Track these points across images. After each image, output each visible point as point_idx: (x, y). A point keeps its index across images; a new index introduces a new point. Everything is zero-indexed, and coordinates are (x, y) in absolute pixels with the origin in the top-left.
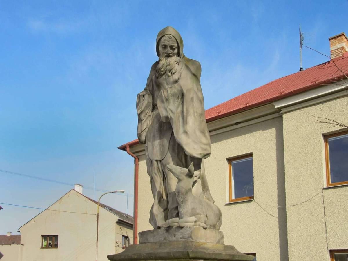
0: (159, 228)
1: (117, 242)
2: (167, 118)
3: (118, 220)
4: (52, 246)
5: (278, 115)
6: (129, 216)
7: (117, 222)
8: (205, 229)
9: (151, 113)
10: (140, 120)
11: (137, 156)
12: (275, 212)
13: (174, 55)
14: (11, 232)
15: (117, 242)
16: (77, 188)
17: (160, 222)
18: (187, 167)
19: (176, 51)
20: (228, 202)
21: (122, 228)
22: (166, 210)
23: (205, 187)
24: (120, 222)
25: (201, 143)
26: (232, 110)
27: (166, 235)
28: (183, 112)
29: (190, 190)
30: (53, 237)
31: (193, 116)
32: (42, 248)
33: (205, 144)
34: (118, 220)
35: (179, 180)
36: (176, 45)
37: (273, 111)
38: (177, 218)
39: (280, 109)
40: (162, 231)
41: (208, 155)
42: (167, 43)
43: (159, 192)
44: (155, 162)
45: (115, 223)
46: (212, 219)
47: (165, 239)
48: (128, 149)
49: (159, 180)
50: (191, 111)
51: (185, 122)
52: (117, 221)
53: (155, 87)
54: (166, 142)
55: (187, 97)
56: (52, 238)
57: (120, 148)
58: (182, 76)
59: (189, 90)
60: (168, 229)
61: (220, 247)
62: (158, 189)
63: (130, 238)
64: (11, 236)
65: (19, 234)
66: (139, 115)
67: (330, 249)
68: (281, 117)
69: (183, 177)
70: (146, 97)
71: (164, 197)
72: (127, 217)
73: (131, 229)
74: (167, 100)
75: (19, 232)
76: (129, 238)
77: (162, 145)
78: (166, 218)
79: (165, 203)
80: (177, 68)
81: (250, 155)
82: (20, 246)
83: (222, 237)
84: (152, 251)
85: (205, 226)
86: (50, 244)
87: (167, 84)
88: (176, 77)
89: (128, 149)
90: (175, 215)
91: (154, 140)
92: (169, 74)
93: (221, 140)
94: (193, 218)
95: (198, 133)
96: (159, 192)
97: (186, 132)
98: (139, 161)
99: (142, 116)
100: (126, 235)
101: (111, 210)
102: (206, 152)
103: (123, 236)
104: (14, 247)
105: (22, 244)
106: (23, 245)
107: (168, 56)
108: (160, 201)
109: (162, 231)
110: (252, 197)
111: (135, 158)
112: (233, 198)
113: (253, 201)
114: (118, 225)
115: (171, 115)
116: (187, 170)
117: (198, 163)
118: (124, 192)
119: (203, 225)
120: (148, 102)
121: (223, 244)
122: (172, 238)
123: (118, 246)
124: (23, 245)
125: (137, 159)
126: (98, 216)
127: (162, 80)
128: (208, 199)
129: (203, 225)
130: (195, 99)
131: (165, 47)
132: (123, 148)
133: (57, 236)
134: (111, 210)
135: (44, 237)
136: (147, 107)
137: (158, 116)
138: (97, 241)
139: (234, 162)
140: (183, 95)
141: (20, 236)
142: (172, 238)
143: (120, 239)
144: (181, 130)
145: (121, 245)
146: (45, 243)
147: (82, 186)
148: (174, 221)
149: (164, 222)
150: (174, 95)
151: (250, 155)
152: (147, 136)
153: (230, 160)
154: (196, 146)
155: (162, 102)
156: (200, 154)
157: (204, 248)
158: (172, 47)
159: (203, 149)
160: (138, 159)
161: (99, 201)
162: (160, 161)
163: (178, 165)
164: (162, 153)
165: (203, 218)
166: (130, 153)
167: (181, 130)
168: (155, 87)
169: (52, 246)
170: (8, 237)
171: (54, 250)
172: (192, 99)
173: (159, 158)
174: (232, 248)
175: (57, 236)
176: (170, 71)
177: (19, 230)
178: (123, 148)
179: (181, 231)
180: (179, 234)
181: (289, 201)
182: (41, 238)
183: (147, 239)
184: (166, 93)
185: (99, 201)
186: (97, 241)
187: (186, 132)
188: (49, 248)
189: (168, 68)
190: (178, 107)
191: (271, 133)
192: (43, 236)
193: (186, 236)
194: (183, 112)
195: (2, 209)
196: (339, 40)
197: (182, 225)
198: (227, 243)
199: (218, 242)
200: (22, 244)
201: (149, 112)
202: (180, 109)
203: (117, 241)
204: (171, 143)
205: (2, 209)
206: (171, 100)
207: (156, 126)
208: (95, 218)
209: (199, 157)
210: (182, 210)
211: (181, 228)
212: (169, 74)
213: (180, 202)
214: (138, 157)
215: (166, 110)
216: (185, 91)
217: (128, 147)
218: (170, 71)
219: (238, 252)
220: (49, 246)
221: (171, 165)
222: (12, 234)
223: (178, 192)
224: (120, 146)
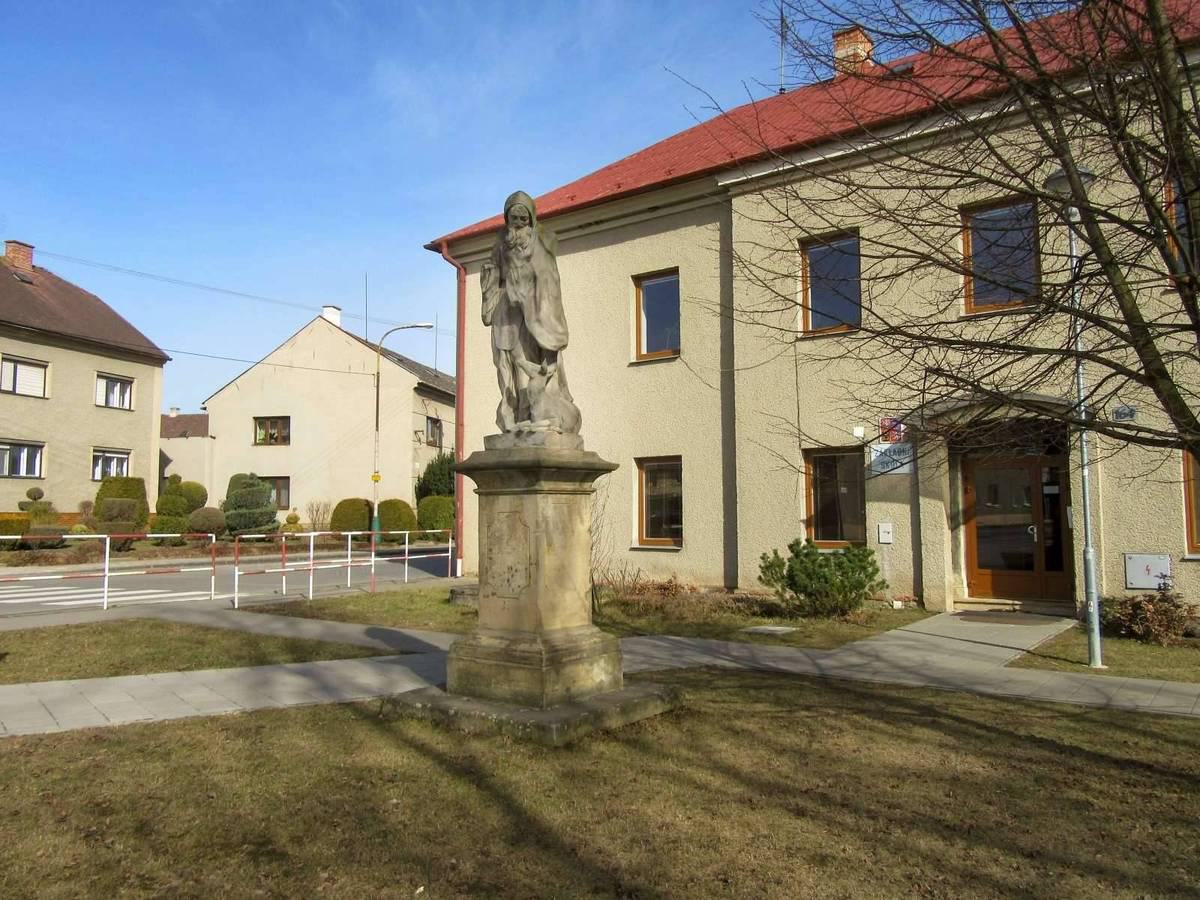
0: (508, 431)
1: (416, 432)
2: (517, 302)
3: (419, 384)
4: (276, 439)
5: (719, 208)
6: (441, 373)
7: (415, 389)
8: (561, 433)
9: (498, 289)
10: (485, 299)
11: (462, 264)
12: (716, 380)
13: (525, 225)
14: (178, 409)
15: (416, 432)
16: (332, 315)
17: (510, 425)
18: (540, 364)
19: (528, 221)
20: (634, 361)
21: (427, 402)
22: (516, 410)
23: (562, 382)
24: (423, 390)
25: (556, 332)
26: (643, 184)
27: (517, 441)
28: (535, 297)
29: (544, 389)
30: (280, 422)
31: (547, 300)
32: (256, 444)
33: (561, 334)
34: (419, 384)
35: (531, 378)
36: (527, 215)
37: (714, 189)
38: (529, 422)
39: (726, 188)
40: (511, 436)
41: (564, 347)
42: (517, 214)
43: (508, 388)
44: (503, 353)
45: (413, 391)
46: (569, 421)
47: (515, 445)
48: (445, 250)
49: (507, 374)
50: (545, 294)
51: (538, 308)
52: (416, 386)
53: (503, 261)
54: (516, 329)
55: (541, 279)
56: (276, 422)
57: (426, 247)
58: (535, 252)
59: (542, 271)
60: (519, 433)
61: (578, 453)
62: (507, 385)
63: (443, 423)
64: (179, 417)
65: (203, 412)
66: (484, 294)
67: (803, 447)
68: (730, 202)
69: (535, 375)
70: (493, 271)
71: (515, 394)
72: (437, 375)
73: (449, 405)
74: (517, 282)
75: (205, 409)
76: (441, 424)
77: (511, 333)
78: (516, 420)
79: (515, 401)
80: (528, 241)
81: (675, 271)
82: (207, 440)
83: (582, 442)
84: (501, 459)
85: (561, 430)
86: (272, 436)
87: (518, 258)
88: (527, 252)
89: (445, 250)
90: (526, 416)
91: (502, 324)
92: (520, 248)
93: (622, 241)
94: (547, 422)
95: (553, 320)
96: (508, 388)
97: (539, 321)
98: (466, 274)
99: (488, 295)
100: (435, 416)
101: (402, 361)
102: (562, 344)
103: (428, 418)
104: (194, 442)
105: (211, 437)
106: (214, 438)
107: (518, 228)
108: (509, 398)
109: (511, 436)
110: (677, 352)
111: (459, 269)
112: (644, 351)
113: (678, 359)
114: (419, 394)
115: (521, 300)
116: (539, 366)
117: (552, 356)
118: (431, 327)
119: (558, 429)
120: (496, 278)
121: (582, 450)
122: (523, 445)
123: (419, 440)
124: (214, 438)
125: (463, 271)
126: (378, 377)
127: (512, 253)
128: (567, 398)
129: (558, 429)
130: (550, 280)
131: (515, 218)
132: (435, 247)
133: (287, 419)
134: (402, 361)
135: (260, 421)
136: (493, 284)
137: (505, 298)
138: (377, 430)
139: (646, 283)
140: (535, 278)
141: (208, 416)
142: (523, 445)
143: (422, 424)
144: (533, 317)
145: (424, 438)
146: (261, 434)
147: (339, 309)
148: (525, 425)
149: (513, 425)
150: (525, 277)
151: (675, 271)
152: (493, 316)
153: (638, 279)
154: (551, 337)
155: (512, 284)
156: (555, 347)
157: (559, 456)
158: (523, 218)
159: (559, 340)
160: (465, 269)
161: (381, 343)
162: (510, 351)
163: (532, 360)
164: (512, 341)
165: (557, 421)
166: (448, 257)
167: (533, 317)
168: (503, 261)
169: (276, 439)
170: (173, 418)
171: (282, 448)
172: (546, 281)
173: (507, 348)
174: (594, 454)
175: (287, 419)
176: (521, 245)
177: (203, 406)
178: (435, 247)
179: (533, 436)
180: (530, 440)
181: (738, 363)
182: (252, 422)
183: (495, 445)
184: (516, 274)
185: (381, 343)
186: (377, 430)
187: (539, 321)
188: (271, 444)
189: (519, 241)
190: (529, 292)
191: (709, 234)
192: (256, 419)
193: (538, 442)
194: (535, 297)
195: (171, 360)
196: (851, 38)
197: (534, 430)
198: (587, 448)
199: (577, 448)
200: (211, 437)
201: (496, 288)
202: (532, 293)
203: (417, 429)
204: (522, 331)
205: (171, 360)
206: (522, 283)
207: (504, 308)
208: (372, 381)
209: (555, 349)
210: (535, 412)
211: (534, 433)
212: (520, 248)
213: (532, 403)
214: (465, 265)
215: (516, 293)
216: (537, 274)
217: (444, 245)
218: (521, 245)
219: (600, 459)
220: (270, 440)
221: (523, 359)
222: (181, 413)
223: (530, 392)
224: (428, 243)
